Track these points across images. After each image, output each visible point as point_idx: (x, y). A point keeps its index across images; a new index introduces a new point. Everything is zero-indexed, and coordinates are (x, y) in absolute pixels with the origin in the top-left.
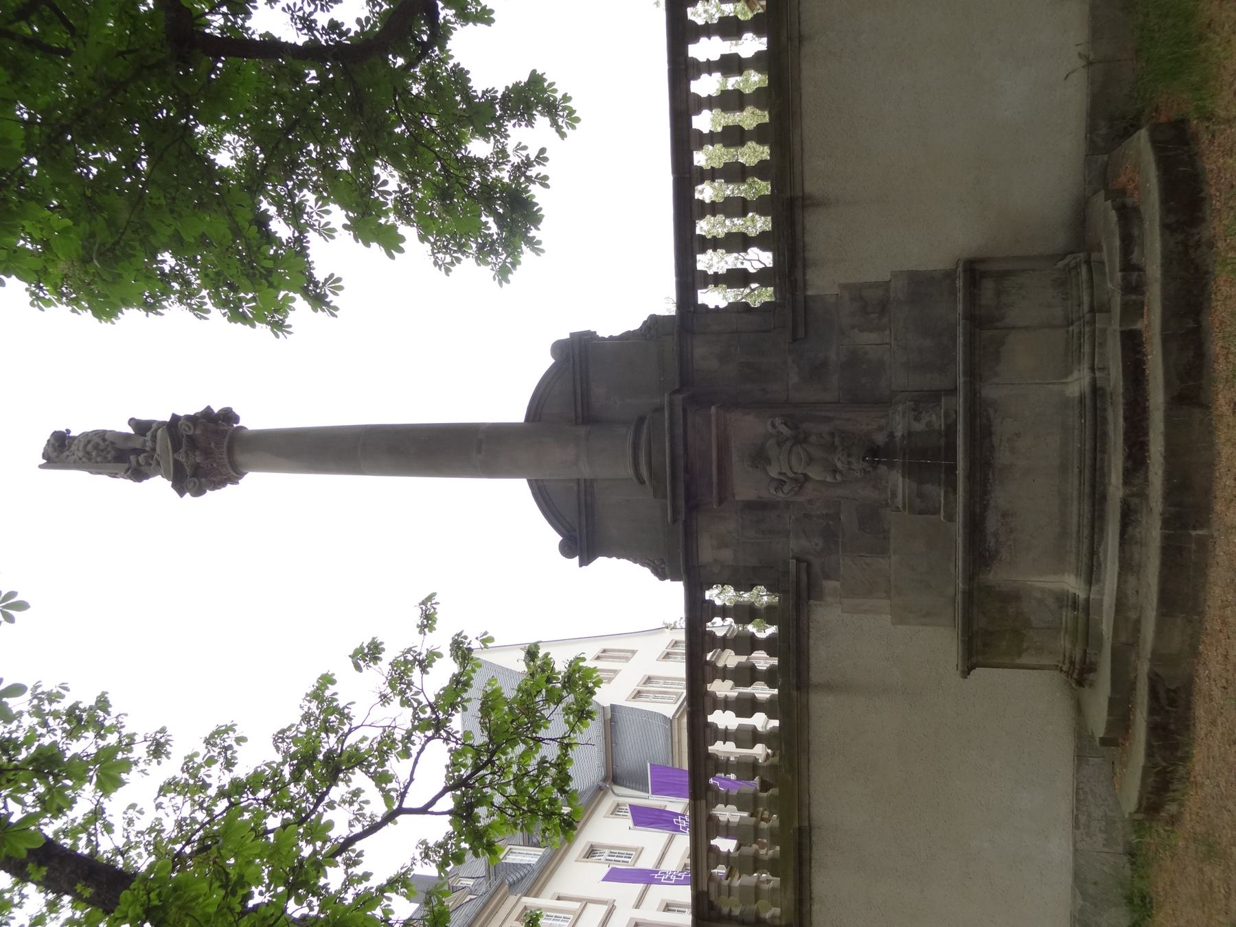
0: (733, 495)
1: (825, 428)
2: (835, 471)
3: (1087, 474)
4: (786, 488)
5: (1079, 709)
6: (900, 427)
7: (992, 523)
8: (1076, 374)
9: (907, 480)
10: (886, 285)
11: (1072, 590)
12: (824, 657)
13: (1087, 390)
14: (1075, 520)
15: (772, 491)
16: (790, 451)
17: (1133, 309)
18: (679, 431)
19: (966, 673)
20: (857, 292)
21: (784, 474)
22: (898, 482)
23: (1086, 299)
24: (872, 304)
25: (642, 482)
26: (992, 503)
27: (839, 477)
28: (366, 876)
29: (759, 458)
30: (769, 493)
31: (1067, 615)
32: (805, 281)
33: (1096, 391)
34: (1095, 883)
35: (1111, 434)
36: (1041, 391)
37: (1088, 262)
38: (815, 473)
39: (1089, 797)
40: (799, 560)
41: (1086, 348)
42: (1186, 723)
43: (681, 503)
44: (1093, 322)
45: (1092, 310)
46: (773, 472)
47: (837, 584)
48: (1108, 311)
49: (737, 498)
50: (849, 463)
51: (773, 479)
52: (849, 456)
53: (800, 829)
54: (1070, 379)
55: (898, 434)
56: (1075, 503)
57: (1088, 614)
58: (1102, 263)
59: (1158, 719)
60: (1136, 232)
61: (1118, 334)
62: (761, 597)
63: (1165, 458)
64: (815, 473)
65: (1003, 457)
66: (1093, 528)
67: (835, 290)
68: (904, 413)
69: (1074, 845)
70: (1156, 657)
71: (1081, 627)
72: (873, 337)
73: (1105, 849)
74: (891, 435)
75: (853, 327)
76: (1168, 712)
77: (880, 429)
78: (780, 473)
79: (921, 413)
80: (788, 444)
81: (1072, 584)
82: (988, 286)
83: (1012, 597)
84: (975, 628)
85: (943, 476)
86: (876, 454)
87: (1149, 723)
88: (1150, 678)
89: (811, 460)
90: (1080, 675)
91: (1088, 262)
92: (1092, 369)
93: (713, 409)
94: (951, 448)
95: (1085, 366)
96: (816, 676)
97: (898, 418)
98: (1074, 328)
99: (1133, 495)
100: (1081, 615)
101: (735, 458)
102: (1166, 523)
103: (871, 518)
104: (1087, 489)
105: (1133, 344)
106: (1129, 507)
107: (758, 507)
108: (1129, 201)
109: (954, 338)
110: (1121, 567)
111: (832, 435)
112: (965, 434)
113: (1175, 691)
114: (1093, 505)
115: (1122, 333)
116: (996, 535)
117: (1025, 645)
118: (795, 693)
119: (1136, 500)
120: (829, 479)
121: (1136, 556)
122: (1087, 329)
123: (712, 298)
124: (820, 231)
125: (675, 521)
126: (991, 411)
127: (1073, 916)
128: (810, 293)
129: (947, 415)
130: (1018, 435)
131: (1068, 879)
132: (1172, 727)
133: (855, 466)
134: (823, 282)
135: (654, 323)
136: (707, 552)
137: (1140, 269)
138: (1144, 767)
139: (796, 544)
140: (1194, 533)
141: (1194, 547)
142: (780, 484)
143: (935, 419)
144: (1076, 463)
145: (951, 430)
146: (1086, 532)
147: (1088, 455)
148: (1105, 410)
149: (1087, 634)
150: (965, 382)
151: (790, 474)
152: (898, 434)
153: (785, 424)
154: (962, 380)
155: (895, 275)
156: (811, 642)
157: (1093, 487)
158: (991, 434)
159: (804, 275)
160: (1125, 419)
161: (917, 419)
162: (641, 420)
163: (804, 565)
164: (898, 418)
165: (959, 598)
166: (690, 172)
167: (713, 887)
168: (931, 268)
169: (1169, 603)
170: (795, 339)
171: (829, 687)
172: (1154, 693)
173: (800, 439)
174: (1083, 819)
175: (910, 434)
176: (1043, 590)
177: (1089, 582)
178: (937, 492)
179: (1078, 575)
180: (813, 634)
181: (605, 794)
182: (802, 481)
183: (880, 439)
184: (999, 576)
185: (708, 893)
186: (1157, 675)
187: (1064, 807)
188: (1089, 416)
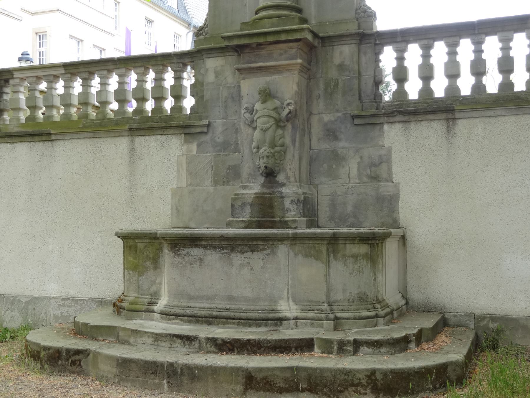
0: (244, 79)
1: (288, 140)
2: (258, 148)
3: (224, 314)
4: (247, 115)
5: (101, 303)
6: (288, 191)
7: (196, 252)
8: (294, 307)
10: (390, 179)
11: (160, 302)
12: (150, 144)
13: (279, 315)
14: (197, 305)
15: (245, 106)
16: (270, 116)
17: (328, 347)
18: (283, 37)
19: (118, 235)
20: (386, 160)
22: (254, 188)
23: (346, 315)
24: (377, 170)
25: (256, 13)
26: (208, 252)
27: (255, 150)
29: (267, 95)
31: (146, 299)
32: (393, 123)
33: (280, 321)
34: (34, 309)
35: (250, 330)
36: (285, 285)
37: (377, 316)
39: (79, 307)
40: (208, 126)
41: (310, 315)
42: (63, 370)
43: (236, 42)
44: (328, 319)
45: (336, 319)
47: (194, 152)
48: (335, 329)
49: (242, 81)
50: (263, 157)
52: (268, 157)
53: (50, 134)
54: (291, 303)
55: (284, 190)
56: (207, 306)
57: (145, 311)
58: (376, 325)
59: (64, 354)
60: (383, 350)
61: (311, 337)
62: (189, 102)
63: (211, 366)
64: (257, 134)
65: (237, 259)
66: (191, 316)
67: (387, 145)
68: (297, 193)
69: (53, 298)
70: (97, 354)
71: (138, 307)
72: (354, 172)
73: (52, 315)
74: (283, 185)
75: (361, 157)
76: (68, 360)
77: (288, 178)
79: (296, 205)
81: (163, 303)
82: (363, 249)
83: (156, 262)
84: (137, 241)
85: (255, 219)
86: (270, 175)
87: (62, 348)
88: (86, 350)
89: (265, 131)
90: (118, 307)
91: (377, 316)
92: (296, 318)
93: (299, 61)
94: (273, 225)
95: (300, 314)
96: (139, 141)
97: (294, 189)
98: (326, 307)
99: (200, 343)
100: (144, 307)
101: (268, 78)
102: (171, 365)
103: (233, 173)
104: (215, 313)
105: (305, 346)
106: (193, 340)
107: (236, 96)
108: (413, 345)
109: (352, 225)
110: (157, 334)
111: (283, 145)
112: (250, 234)
113: (80, 365)
114: (205, 317)
115: (312, 339)
116: (188, 254)
117: (131, 272)
118: (127, 127)
119: (197, 345)
121: (163, 344)
122: (323, 315)
123: (388, 58)
124: (430, 131)
125: (224, 38)
126: (268, 251)
127: (17, 296)
128: (386, 126)
129: (294, 221)
130: (252, 269)
131: (36, 294)
132: (60, 362)
133: (262, 161)
134: (393, 135)
135: (371, 16)
136: (213, 63)
137: (356, 351)
138: (40, 344)
139: (218, 124)
140: (165, 382)
141: (157, 381)
142: (251, 111)
143: (292, 213)
144: (233, 306)
145: (284, 224)
146: (189, 312)
147: (237, 315)
148: (266, 325)
149: (134, 311)
150: (288, 234)
151: (256, 117)
152: (284, 190)
153: (290, 113)
154: (290, 232)
155: (397, 186)
156: (159, 137)
157: (216, 317)
158: (253, 251)
159: (399, 122)
160: (249, 340)
162: (299, 11)
163: (205, 130)
165: (190, 232)
166: (480, 33)
167: (17, 81)
168: (401, 210)
169: (124, 364)
170: (353, 117)
171: (132, 149)
172: (78, 352)
173: (279, 123)
174: (67, 303)
175: (283, 197)
176: (160, 283)
177: (161, 313)
178: (246, 215)
179: (167, 306)
180: (163, 137)
181: (187, 28)
182: (252, 124)
183: (281, 178)
184: (167, 256)
185: (13, 78)
186: (88, 355)
187: (73, 292)
188: (262, 316)
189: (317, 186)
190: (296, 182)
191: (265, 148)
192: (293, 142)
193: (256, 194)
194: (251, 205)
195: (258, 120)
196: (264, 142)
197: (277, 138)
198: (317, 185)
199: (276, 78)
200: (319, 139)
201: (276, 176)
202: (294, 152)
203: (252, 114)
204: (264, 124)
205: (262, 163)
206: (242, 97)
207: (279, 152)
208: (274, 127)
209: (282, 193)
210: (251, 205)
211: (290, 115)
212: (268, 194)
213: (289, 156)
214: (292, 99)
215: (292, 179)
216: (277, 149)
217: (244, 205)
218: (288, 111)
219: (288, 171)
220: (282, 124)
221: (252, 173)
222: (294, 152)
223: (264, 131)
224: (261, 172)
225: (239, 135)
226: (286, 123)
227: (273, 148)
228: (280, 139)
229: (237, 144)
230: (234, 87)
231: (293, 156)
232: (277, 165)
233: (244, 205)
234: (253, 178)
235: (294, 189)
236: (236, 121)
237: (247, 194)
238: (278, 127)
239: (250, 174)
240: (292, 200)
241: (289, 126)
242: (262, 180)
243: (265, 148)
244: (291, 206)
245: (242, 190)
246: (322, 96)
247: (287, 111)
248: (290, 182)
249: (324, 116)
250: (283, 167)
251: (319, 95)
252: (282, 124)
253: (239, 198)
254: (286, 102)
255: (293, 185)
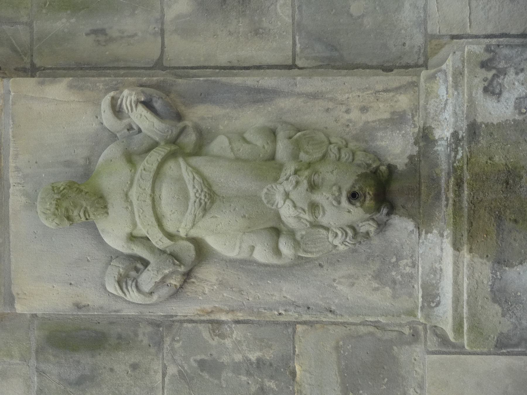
1: (252, 119)
4: (148, 278)
6: (448, 115)
9: (466, 256)
15: (112, 288)
21: (145, 240)
27: (286, 248)
28: (447, 138)
29: (77, 196)
30: (102, 295)
38: (225, 235)
46: (114, 234)
49: (19, 308)
50: (314, 207)
51: (117, 255)
52: (313, 187)
55: (443, 133)
64: (225, 235)
68: (458, 74)
74: (426, 137)
77: (398, 120)
78: (132, 238)
79: (502, 72)
80: (153, 159)
86: (383, 190)
89: (211, 198)
97: (442, 90)
111: (272, 134)
120: (262, 255)
151: (159, 241)
153: (148, 105)
161: (491, 90)
164: (442, 90)
173: (185, 144)
175: (474, 129)
183: (397, 148)
189: (433, 37)
190: (414, 85)
191: (279, 198)
192: (259, 96)
193: (456, 247)
194: (501, 261)
195: (170, 227)
196: (253, 199)
197: (243, 150)
198: (430, 37)
199: (17, 169)
200: (257, 32)
201: (391, 168)
202: (299, 95)
203: (146, 263)
204: (187, 198)
205: (340, 214)
206: (78, 306)
207: (297, 148)
208: (195, 161)
209: (455, 134)
210: (501, 261)
211: (158, 105)
212: (458, 192)
213: (314, 115)
214: (97, 104)
215: (403, 101)
216: (282, 149)
217: (500, 295)
218: (141, 110)
219: (370, 117)
220: (190, 139)
221: (375, 266)
222: (299, 95)
223: (213, 202)
224: (370, 227)
225: (225, 359)
226: (187, 123)
227: (281, 167)
228: (248, 142)
229: (260, 363)
230: (41, 373)
231: (315, 96)
232: (345, 155)
233: (500, 295)
234: (396, 265)
235: (442, 91)
236: (172, 370)
237: (456, 283)
238: (199, 149)
239: (377, 276)
240: (486, 90)
241: (199, 113)
242: (402, 226)
243: (279, 198)
244: (510, 97)
245: (439, 310)
246: (98, 23)
247: (143, 119)
248: (416, 109)
249: (170, 15)
250: (356, 138)
251: (95, 32)
252: (190, 139)
253: (473, 315)
254: (107, 118)
255: (428, 94)
